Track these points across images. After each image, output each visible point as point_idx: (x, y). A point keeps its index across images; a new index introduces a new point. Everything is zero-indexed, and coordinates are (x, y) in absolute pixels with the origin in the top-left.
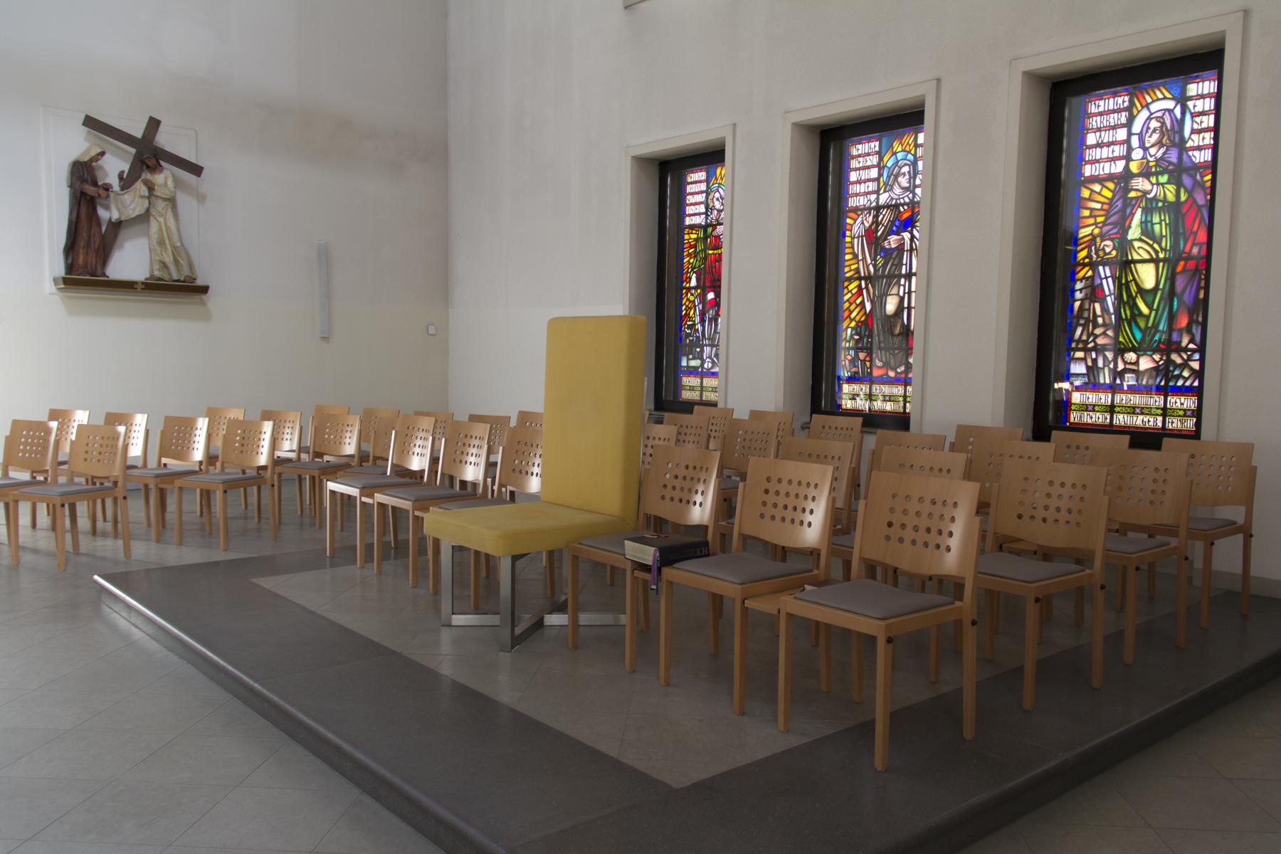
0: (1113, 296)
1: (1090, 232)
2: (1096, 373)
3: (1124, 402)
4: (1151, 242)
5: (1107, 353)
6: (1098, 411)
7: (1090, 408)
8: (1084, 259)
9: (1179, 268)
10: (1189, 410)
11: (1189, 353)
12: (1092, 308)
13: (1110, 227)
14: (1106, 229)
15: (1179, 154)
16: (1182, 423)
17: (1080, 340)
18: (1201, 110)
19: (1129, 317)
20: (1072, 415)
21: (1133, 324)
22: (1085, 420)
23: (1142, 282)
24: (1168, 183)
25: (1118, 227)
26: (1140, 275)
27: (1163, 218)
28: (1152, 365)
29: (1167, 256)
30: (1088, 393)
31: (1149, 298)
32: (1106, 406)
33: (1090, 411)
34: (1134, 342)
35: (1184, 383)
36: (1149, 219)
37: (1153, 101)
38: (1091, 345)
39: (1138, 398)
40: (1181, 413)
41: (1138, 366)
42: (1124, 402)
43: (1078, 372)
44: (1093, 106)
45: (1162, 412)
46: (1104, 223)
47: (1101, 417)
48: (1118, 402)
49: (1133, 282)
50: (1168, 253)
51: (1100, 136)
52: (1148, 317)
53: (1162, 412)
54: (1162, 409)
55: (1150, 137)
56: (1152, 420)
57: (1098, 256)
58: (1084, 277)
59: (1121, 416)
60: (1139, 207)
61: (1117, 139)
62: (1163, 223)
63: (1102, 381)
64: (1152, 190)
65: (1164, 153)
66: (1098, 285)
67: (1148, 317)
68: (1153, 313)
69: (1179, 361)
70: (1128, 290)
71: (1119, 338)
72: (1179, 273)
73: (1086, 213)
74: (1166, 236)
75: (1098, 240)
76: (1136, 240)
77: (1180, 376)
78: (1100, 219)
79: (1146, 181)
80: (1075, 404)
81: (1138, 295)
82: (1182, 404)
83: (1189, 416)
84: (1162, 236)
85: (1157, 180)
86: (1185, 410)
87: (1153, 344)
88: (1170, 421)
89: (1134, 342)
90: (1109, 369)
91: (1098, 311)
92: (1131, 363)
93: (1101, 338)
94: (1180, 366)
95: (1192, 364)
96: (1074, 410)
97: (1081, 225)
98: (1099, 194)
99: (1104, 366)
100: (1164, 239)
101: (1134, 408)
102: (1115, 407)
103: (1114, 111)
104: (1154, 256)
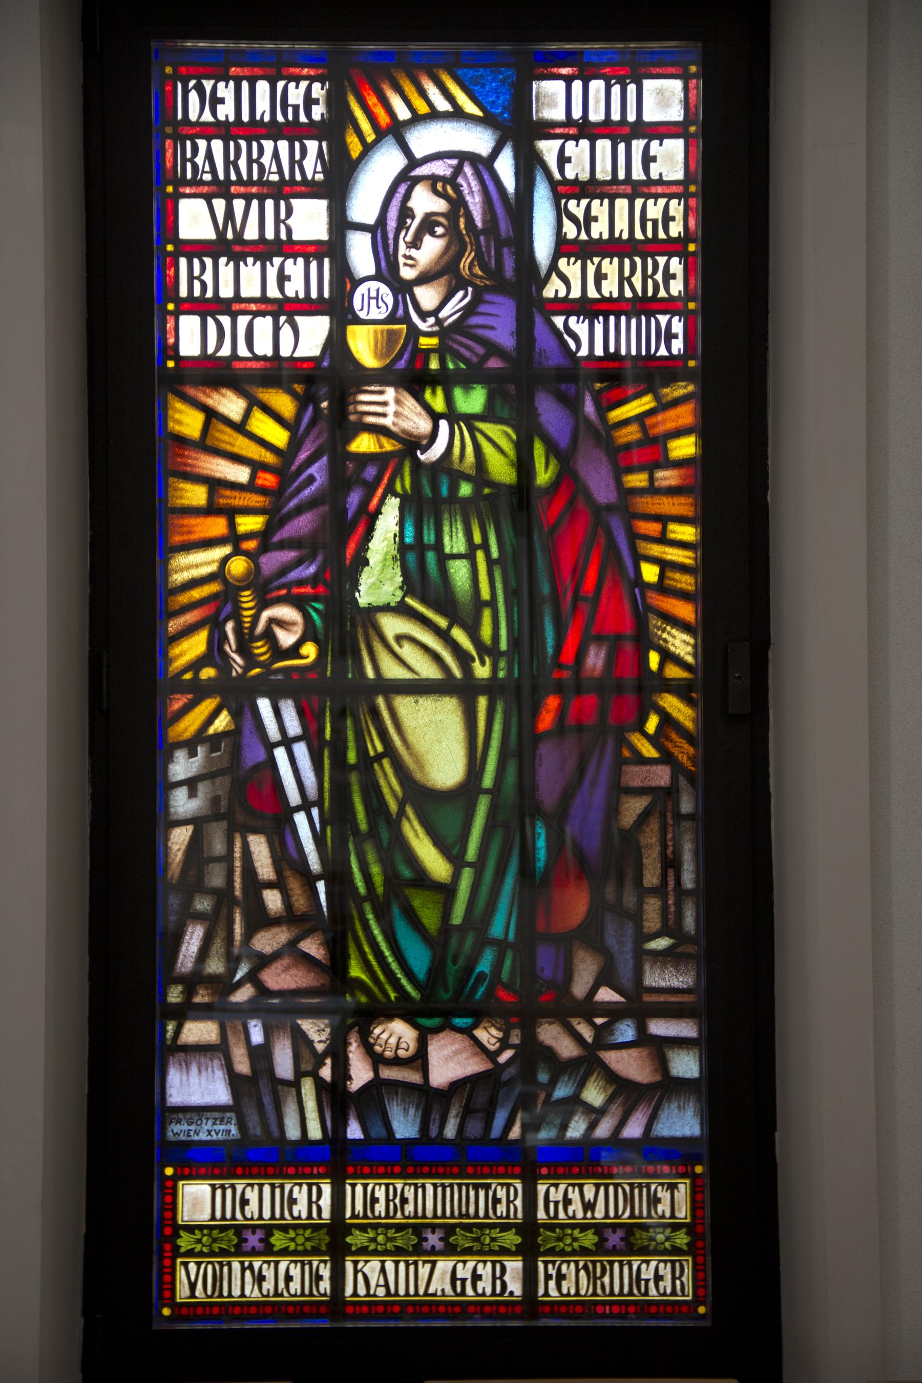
0: (315, 812)
1: (213, 568)
2: (267, 1100)
3: (380, 1208)
4: (443, 623)
5: (307, 1025)
6: (284, 1252)
7: (253, 1240)
8: (197, 665)
9: (546, 720)
10: (614, 1227)
11: (599, 1021)
12: (237, 855)
13: (290, 555)
14: (272, 561)
15: (518, 319)
16: (593, 1278)
17: (192, 982)
18: (585, 176)
19: (380, 890)
20: (181, 1273)
21: (396, 911)
22: (236, 1292)
23: (421, 767)
24: (488, 415)
25: (320, 558)
26: (411, 738)
27: (477, 539)
28: (473, 1066)
29: (501, 674)
30: (240, 1184)
31: (450, 826)
32: (316, 1228)
33: (254, 1253)
34: (404, 981)
35: (592, 1126)
36: (429, 537)
37: (417, 119)
38: (243, 995)
39: (430, 1190)
40: (589, 1239)
41: (425, 1070)
42: (380, 1208)
43: (196, 1098)
44: (193, 96)
45: (518, 1240)
46: (265, 537)
47: (295, 1271)
48: (359, 1207)
49: (386, 763)
50: (502, 664)
51: (229, 213)
52: (447, 891)
53: (518, 1240)
54: (520, 1229)
55: (416, 243)
56: (485, 1271)
57: (250, 660)
58: (200, 737)
59: (372, 1267)
60: (390, 490)
61: (296, 237)
62: (480, 555)
63: (293, 1133)
64: (433, 436)
65: (468, 311)
66: (257, 767)
67: (447, 891)
68: (467, 876)
69: (567, 1049)
70: (372, 792)
71: (345, 968)
72: (547, 734)
73: (196, 495)
74: (492, 604)
75: (247, 598)
76: (386, 608)
77: (575, 1102)
78: (249, 524)
79: (410, 402)
80: (190, 1229)
81: (409, 811)
82: (589, 1206)
83: (614, 1251)
84: (478, 604)
85: (449, 400)
86: (599, 1229)
87: (474, 989)
88: (552, 1271)
89: (404, 981)
90: (320, 1084)
91: (264, 867)
92: (397, 1062)
93: (277, 966)
94: (572, 1065)
95: (614, 1059)
96: (190, 1253)
97: (177, 539)
98: (240, 428)
99: (299, 1074)
100: (487, 614)
101: (418, 1230)
102: (348, 1230)
103: (274, 131)
104: (457, 673)
